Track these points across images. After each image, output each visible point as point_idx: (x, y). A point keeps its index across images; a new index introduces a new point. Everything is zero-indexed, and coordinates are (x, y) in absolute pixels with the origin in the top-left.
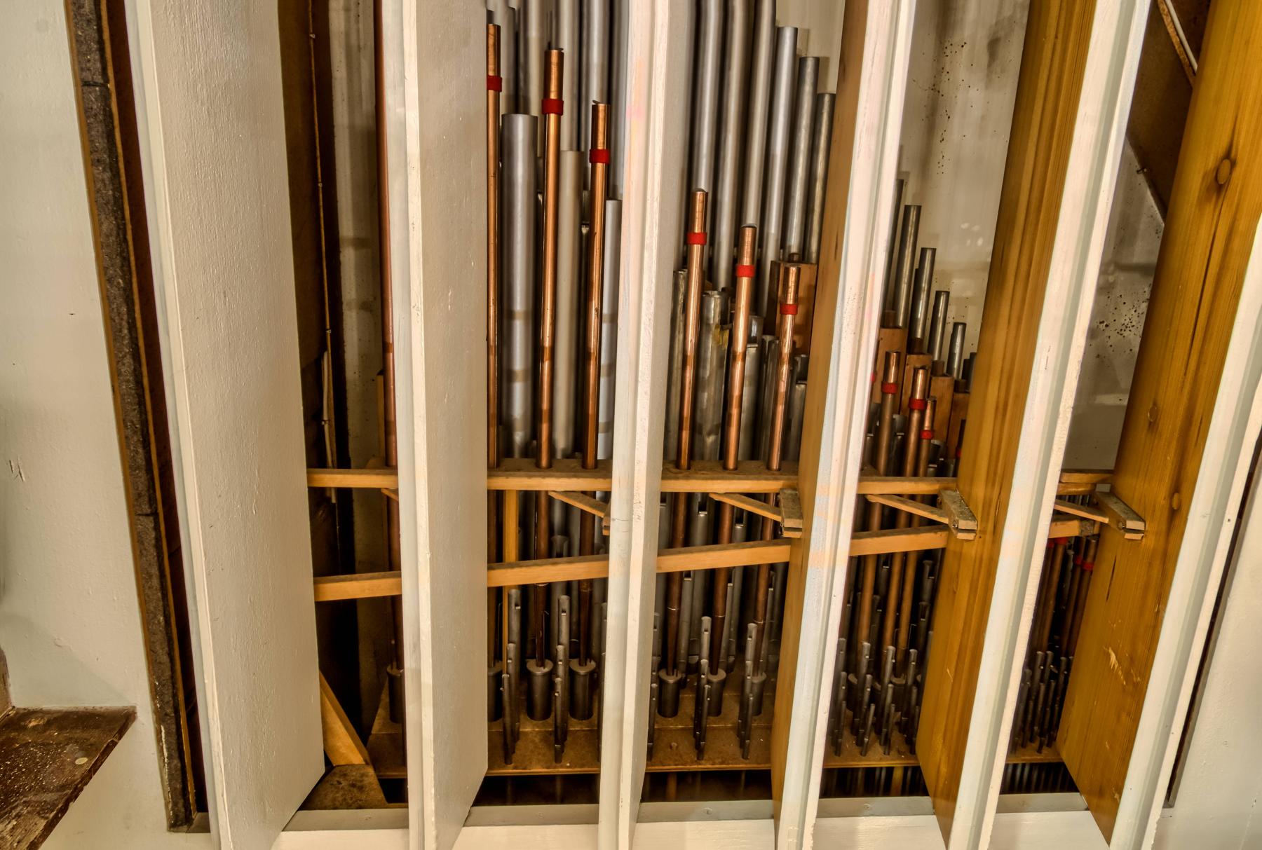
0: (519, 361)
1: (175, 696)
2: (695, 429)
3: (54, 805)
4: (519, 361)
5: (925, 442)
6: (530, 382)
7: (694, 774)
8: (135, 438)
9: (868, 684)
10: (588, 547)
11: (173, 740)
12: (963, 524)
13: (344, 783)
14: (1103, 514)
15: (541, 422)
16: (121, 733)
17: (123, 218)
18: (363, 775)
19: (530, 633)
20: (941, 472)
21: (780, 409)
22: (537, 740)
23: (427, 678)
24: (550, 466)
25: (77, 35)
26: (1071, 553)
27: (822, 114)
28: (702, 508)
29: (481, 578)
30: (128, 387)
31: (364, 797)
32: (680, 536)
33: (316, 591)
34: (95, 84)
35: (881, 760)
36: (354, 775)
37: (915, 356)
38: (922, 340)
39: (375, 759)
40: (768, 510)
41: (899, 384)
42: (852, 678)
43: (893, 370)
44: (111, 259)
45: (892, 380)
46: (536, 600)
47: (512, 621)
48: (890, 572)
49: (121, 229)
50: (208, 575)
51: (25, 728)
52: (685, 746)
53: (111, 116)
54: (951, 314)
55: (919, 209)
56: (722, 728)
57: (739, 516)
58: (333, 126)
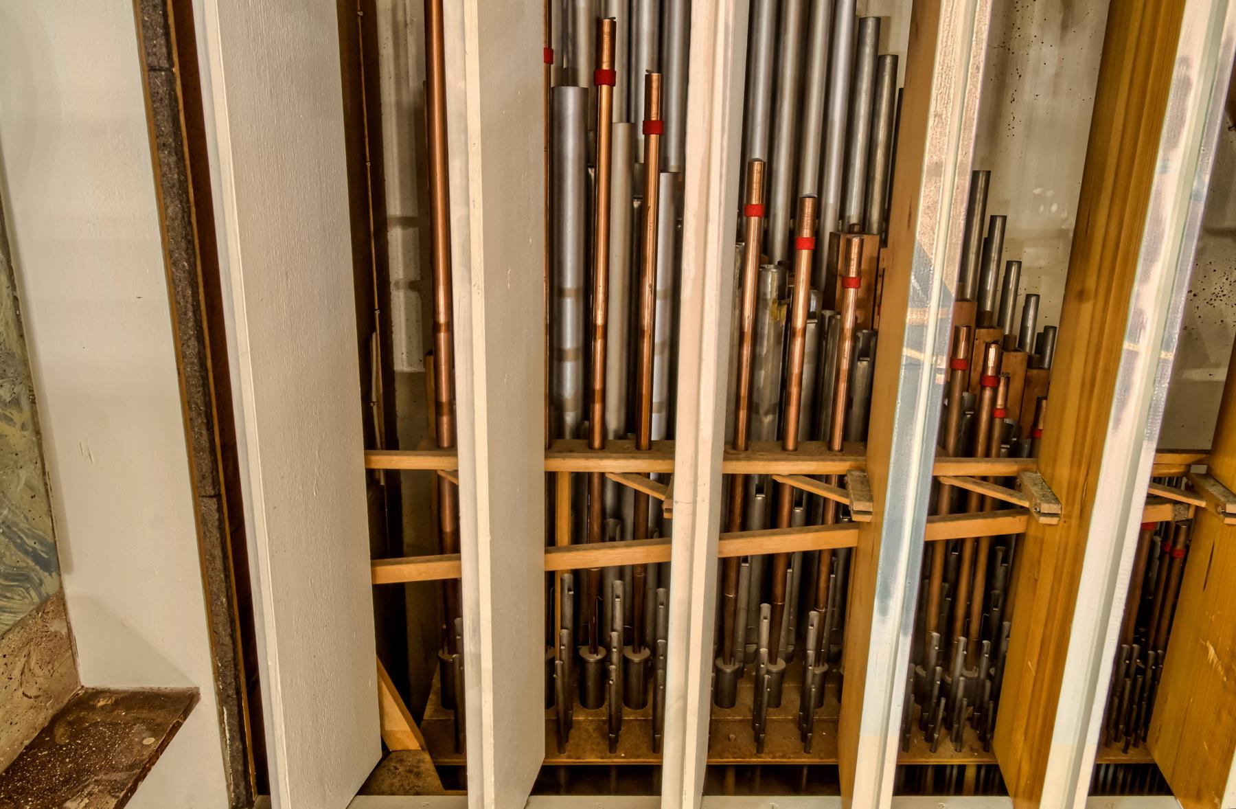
0: (570, 340)
1: (237, 677)
2: (753, 408)
3: (124, 785)
4: (570, 340)
5: (997, 421)
6: (581, 361)
7: (753, 768)
8: (200, 420)
9: (937, 677)
10: (642, 530)
11: (235, 722)
12: (1046, 508)
13: (401, 769)
14: (1200, 497)
15: (594, 402)
16: (186, 714)
17: (188, 201)
18: (419, 761)
19: (582, 618)
20: (1014, 453)
21: (843, 387)
22: (591, 728)
23: (487, 663)
24: (603, 447)
25: (143, 20)
26: (1158, 539)
27: (883, 76)
28: (759, 491)
29: (537, 561)
30: (193, 370)
31: (420, 784)
32: (738, 519)
33: (374, 574)
34: (161, 69)
35: (952, 757)
36: (411, 760)
37: (984, 331)
38: (991, 313)
39: (430, 744)
40: (831, 491)
41: (969, 360)
42: (922, 672)
43: (963, 345)
44: (176, 243)
45: (961, 355)
46: (588, 585)
47: (565, 607)
48: (960, 559)
49: (186, 212)
50: (272, 556)
51: (94, 708)
52: (743, 737)
53: (176, 100)
54: (1022, 285)
55: (988, 174)
56: (782, 718)
57: (800, 498)
58: (380, 104)
